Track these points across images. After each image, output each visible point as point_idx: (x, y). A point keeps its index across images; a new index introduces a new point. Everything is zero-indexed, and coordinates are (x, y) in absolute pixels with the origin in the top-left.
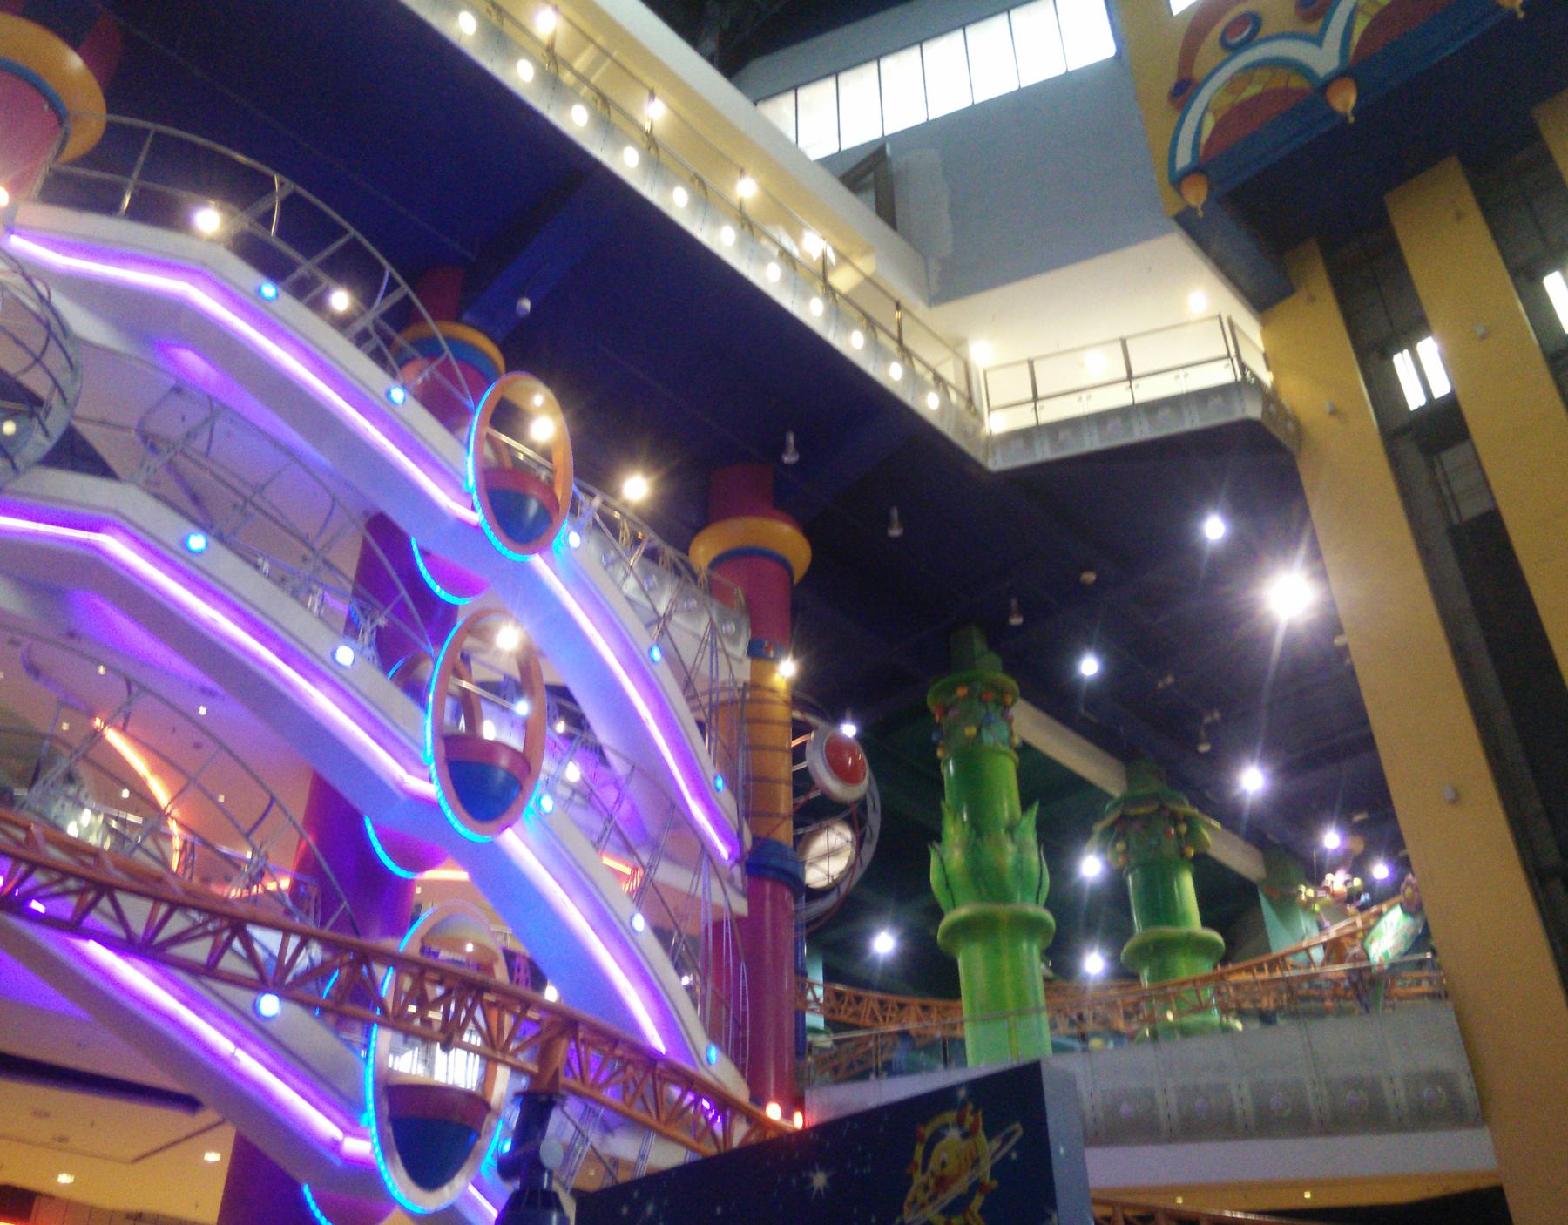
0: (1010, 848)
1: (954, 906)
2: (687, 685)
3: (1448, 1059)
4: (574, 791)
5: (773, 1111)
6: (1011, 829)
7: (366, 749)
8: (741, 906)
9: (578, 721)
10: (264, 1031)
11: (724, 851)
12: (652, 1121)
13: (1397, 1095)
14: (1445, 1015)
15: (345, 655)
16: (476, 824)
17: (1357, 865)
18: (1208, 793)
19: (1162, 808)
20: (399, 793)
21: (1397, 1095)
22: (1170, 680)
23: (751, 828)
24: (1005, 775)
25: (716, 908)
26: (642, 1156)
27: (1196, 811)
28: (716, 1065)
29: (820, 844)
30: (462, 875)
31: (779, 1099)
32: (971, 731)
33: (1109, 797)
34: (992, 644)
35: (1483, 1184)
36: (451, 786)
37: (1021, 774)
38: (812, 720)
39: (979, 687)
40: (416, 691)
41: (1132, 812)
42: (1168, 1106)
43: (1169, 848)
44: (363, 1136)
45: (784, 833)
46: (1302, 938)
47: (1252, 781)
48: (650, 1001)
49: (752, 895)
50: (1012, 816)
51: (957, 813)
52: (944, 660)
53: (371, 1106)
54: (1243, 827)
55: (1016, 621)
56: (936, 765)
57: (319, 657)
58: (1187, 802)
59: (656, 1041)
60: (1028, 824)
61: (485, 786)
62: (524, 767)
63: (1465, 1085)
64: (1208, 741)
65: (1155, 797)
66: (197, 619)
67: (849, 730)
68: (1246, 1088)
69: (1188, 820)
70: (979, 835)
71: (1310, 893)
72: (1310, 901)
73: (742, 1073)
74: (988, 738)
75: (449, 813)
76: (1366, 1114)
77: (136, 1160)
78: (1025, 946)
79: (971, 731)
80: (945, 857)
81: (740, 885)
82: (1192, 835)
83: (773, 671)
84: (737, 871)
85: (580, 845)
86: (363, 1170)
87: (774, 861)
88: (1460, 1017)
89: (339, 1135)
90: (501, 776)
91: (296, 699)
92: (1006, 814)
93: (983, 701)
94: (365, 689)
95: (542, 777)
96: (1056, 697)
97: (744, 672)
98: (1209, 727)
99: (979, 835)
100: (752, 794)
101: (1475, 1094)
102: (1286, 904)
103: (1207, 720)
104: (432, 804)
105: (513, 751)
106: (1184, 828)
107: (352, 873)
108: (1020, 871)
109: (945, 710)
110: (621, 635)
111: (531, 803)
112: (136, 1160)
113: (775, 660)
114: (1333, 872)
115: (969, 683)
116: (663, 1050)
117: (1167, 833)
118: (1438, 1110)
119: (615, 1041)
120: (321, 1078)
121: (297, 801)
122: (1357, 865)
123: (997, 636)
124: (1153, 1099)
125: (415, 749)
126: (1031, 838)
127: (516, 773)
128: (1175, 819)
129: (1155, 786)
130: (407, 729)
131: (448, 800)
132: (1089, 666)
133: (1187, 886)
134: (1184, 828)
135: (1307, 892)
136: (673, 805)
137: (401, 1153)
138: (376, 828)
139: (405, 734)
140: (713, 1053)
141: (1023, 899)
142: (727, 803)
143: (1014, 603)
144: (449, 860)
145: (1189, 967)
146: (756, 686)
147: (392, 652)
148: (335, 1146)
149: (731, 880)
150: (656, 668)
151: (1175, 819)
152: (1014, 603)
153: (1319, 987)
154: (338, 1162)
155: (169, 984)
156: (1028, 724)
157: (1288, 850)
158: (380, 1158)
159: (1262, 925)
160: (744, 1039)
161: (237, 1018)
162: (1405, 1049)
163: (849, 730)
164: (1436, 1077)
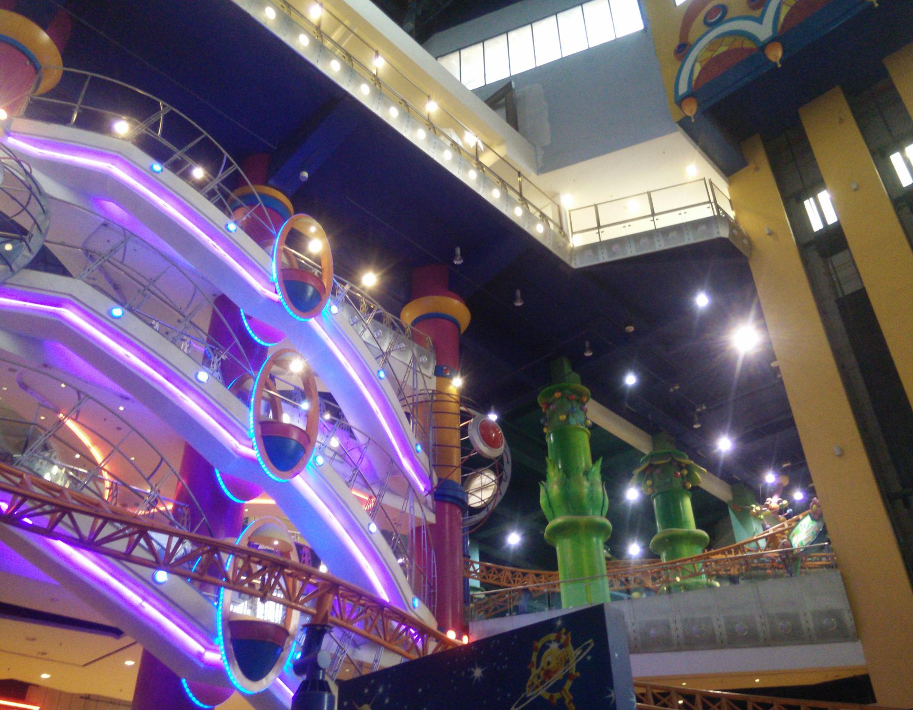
1: (554, 517)
3: (837, 602)
4: (336, 453)
5: (451, 635)
6: (586, 473)
7: (215, 430)
8: (431, 518)
9: (337, 413)
12: (382, 641)
13: (808, 623)
15: (203, 376)
17: (785, 492)
19: (673, 460)
21: (808, 623)
22: (677, 387)
23: (437, 474)
24: (583, 442)
25: (418, 519)
26: (376, 661)
28: (418, 609)
29: (477, 483)
31: (454, 628)
33: (643, 454)
34: (574, 368)
35: (858, 673)
37: (592, 441)
38: (471, 411)
39: (567, 392)
40: (244, 396)
42: (677, 631)
43: (677, 483)
46: (753, 534)
49: (438, 512)
50: (587, 465)
51: (555, 464)
53: (220, 633)
54: (720, 470)
55: (588, 354)
56: (543, 436)
58: (687, 456)
60: (596, 470)
61: (283, 449)
63: (848, 617)
64: (699, 422)
66: (118, 356)
69: (688, 467)
71: (758, 508)
72: (758, 513)
73: (433, 613)
74: (573, 421)
76: (791, 634)
78: (594, 539)
81: (430, 505)
82: (690, 477)
83: (449, 384)
84: (429, 498)
86: (216, 670)
87: (451, 493)
89: (202, 650)
92: (584, 465)
96: (611, 397)
98: (700, 414)
100: (437, 453)
101: (853, 623)
102: (744, 515)
103: (699, 410)
104: (254, 461)
106: (685, 472)
107: (208, 501)
108: (592, 498)
109: (548, 405)
111: (311, 459)
113: (450, 377)
114: (771, 497)
115: (561, 390)
117: (676, 475)
121: (176, 460)
122: (785, 492)
123: (578, 363)
124: (669, 627)
126: (598, 478)
128: (680, 467)
132: (630, 380)
133: (687, 503)
135: (756, 508)
136: (392, 461)
138: (222, 474)
140: (417, 602)
141: (594, 514)
145: (688, 551)
146: (440, 393)
147: (231, 375)
148: (200, 656)
149: (426, 504)
151: (680, 467)
152: (587, 344)
153: (763, 562)
154: (202, 665)
156: (596, 413)
157: (745, 484)
158: (226, 663)
159: (731, 527)
160: (434, 593)
162: (813, 597)
164: (831, 613)
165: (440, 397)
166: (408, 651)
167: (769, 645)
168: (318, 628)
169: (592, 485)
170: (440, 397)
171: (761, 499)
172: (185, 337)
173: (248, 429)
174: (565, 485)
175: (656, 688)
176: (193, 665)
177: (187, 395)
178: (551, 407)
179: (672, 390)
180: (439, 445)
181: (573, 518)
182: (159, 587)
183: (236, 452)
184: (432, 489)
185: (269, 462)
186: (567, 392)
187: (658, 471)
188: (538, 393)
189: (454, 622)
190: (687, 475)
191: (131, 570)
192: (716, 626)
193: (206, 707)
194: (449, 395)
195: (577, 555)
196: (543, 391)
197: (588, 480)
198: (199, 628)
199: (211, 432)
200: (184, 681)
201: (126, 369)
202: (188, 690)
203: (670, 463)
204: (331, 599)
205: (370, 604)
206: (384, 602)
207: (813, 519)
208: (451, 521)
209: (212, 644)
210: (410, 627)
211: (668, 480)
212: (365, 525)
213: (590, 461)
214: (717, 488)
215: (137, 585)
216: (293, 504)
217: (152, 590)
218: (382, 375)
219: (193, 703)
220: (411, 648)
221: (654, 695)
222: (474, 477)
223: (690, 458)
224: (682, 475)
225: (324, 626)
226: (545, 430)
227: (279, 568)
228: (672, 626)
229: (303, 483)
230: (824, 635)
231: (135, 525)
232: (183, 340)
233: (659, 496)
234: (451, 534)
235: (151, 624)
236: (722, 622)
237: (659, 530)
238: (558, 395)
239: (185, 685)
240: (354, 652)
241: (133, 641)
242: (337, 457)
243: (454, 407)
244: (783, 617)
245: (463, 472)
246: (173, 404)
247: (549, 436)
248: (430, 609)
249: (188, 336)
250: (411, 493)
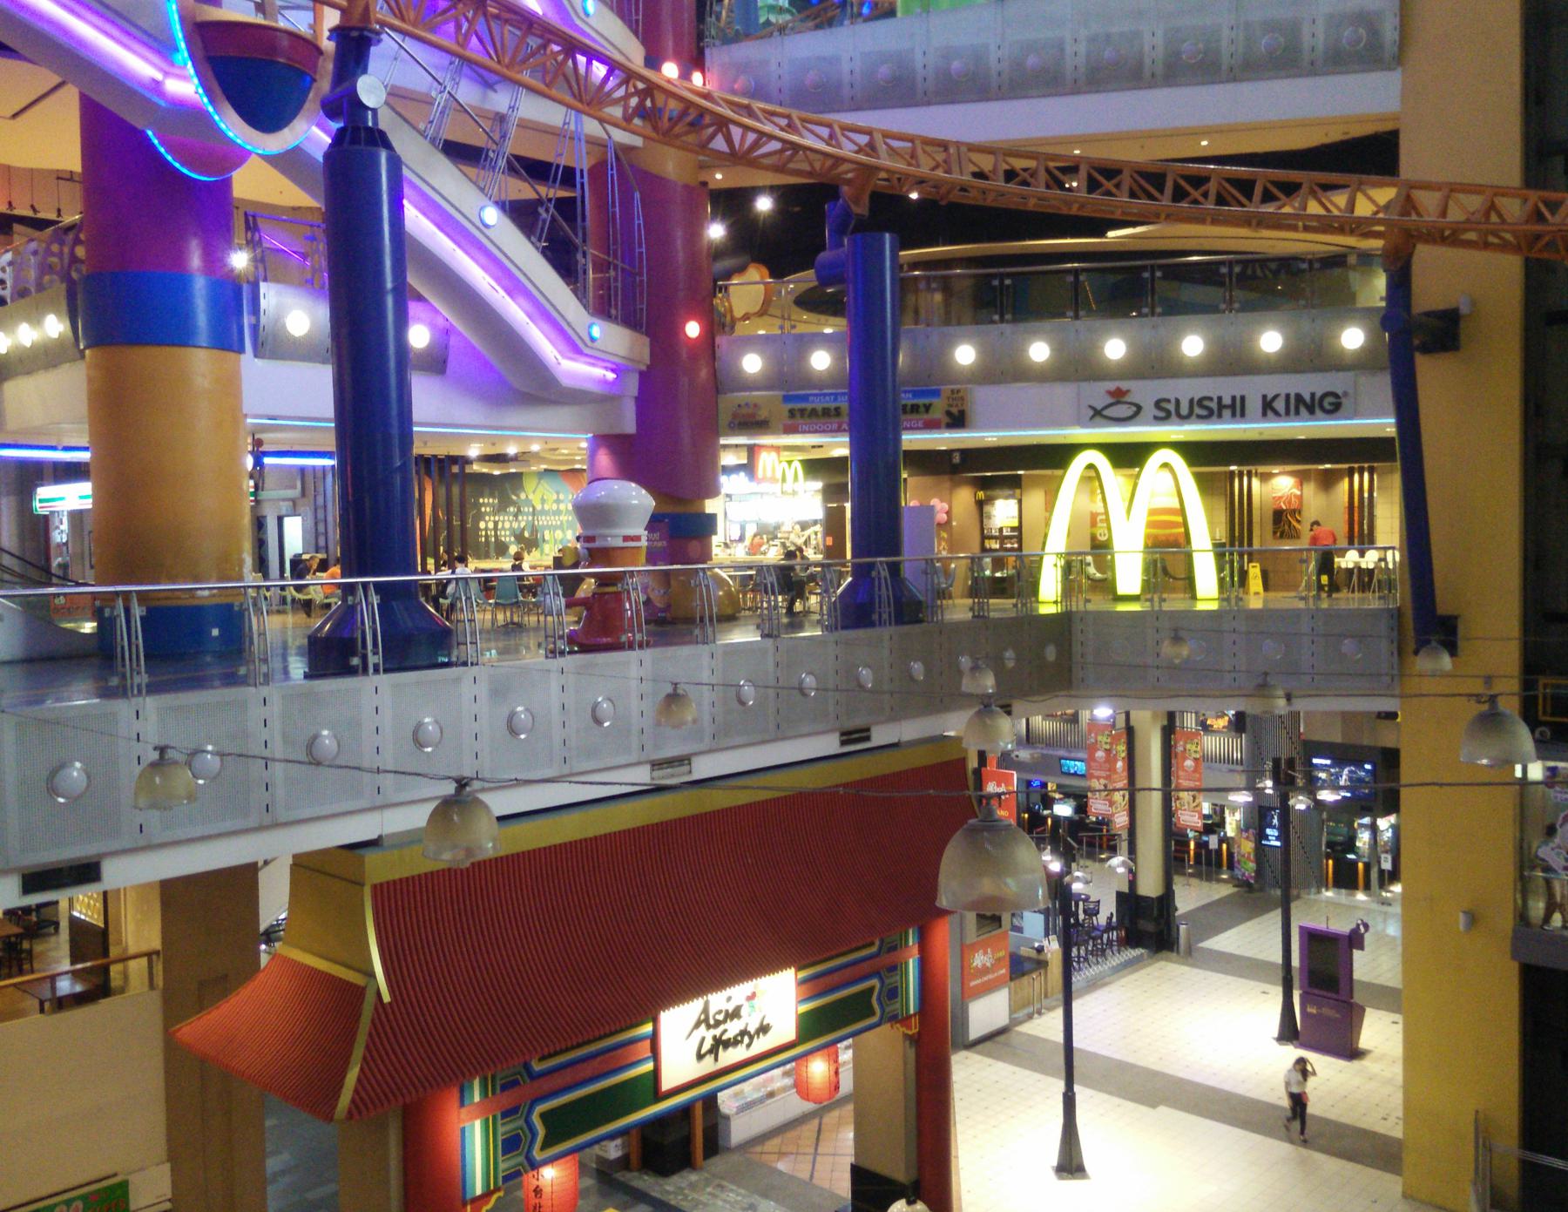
5: (670, 70)
12: (493, 64)
26: (512, 108)
31: (677, 57)
44: (185, 78)
53: (182, 45)
63: (1390, 33)
73: (636, 33)
77: (15, 116)
89: (159, 76)
112: (15, 116)
124: (1062, 50)
137: (229, 98)
148: (156, 86)
154: (162, 103)
158: (205, 100)
167: (1235, 80)
168: (355, 34)
175: (1054, 157)
189: (676, 44)
192: (1147, 48)
198: (138, 34)
206: (534, 14)
209: (172, 64)
210: (549, 41)
220: (555, 76)
221: (1048, 171)
225: (361, 29)
228: (1069, 50)
230: (1338, 60)
235: (46, 27)
236: (1159, 40)
240: (484, 97)
248: (630, 27)
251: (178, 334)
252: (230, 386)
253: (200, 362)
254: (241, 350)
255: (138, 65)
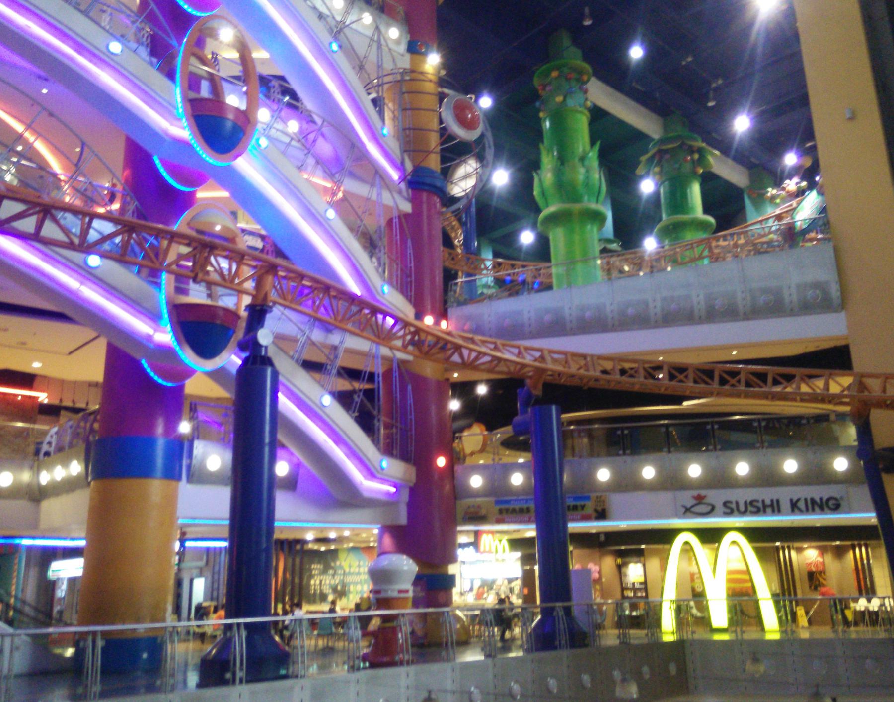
0: (582, 170)
1: (547, 206)
2: (360, 68)
3: (826, 274)
4: (292, 139)
5: (429, 320)
6: (582, 159)
7: (139, 109)
8: (407, 207)
9: (294, 96)
10: (91, 274)
11: (395, 175)
13: (791, 296)
14: (829, 249)
15: (116, 47)
16: (216, 155)
18: (714, 135)
19: (683, 144)
20: (166, 138)
21: (791, 296)
22: (690, 59)
23: (412, 160)
24: (581, 124)
25: (386, 207)
26: (341, 342)
27: (704, 145)
28: (390, 296)
29: (461, 171)
30: (225, 194)
31: (432, 313)
32: (559, 99)
33: (653, 140)
34: (575, 42)
36: (197, 132)
37: (591, 123)
38: (446, 91)
39: (566, 70)
40: (171, 75)
41: (664, 147)
42: (656, 308)
43: (687, 167)
44: (164, 332)
45: (434, 162)
46: (763, 220)
47: (742, 124)
48: (344, 263)
49: (415, 200)
50: (584, 150)
51: (550, 150)
52: (541, 52)
54: (733, 152)
55: (587, 23)
56: (539, 122)
57: (98, 49)
58: (700, 140)
59: (355, 288)
60: (593, 156)
61: (219, 130)
62: (245, 121)
63: (835, 291)
64: (714, 99)
65: (679, 137)
66: (18, 27)
67: (486, 102)
68: (702, 297)
69: (700, 151)
70: (563, 163)
71: (774, 192)
72: (773, 198)
74: (570, 102)
75: (198, 149)
76: (774, 307)
78: (589, 227)
79: (559, 99)
80: (542, 178)
81: (405, 194)
82: (702, 160)
83: (424, 61)
84: (403, 186)
85: (289, 169)
86: (165, 350)
87: (428, 181)
88: (836, 250)
90: (229, 125)
91: (90, 78)
92: (581, 149)
93: (568, 79)
94: (131, 69)
95: (259, 127)
96: (615, 73)
97: (405, 62)
98: (716, 89)
99: (563, 163)
100: (411, 139)
101: (839, 294)
102: (760, 200)
103: (714, 85)
104: (187, 144)
105: (237, 110)
106: (696, 156)
107: (154, 193)
108: (587, 184)
109: (544, 87)
110: (309, 34)
111: (253, 141)
113: (425, 55)
114: (790, 179)
115: (558, 68)
116: (359, 294)
117: (686, 160)
118: (817, 303)
119: (327, 288)
120: (134, 301)
121: (117, 155)
123: (578, 34)
124: (647, 306)
125: (171, 109)
126: (595, 163)
127: (240, 123)
128: (691, 150)
129: (680, 130)
130: (162, 95)
131: (197, 141)
132: (636, 52)
133: (695, 191)
134: (696, 156)
135: (772, 192)
136: (353, 146)
138: (161, 161)
139: (164, 100)
140: (386, 288)
141: (589, 201)
142: (394, 146)
143: (587, 10)
144: (211, 182)
145: (690, 236)
146: (414, 74)
147: (160, 52)
148: (149, 338)
149: (400, 192)
150: (335, 56)
151: (691, 150)
152: (587, 10)
154: (152, 346)
155: (31, 249)
156: (599, 93)
160: (411, 282)
161: (63, 261)
163: (486, 102)
164: (816, 285)
165: (415, 75)
166: (316, 311)
167: (748, 319)
169: (587, 171)
170: (415, 75)
171: (778, 183)
172: (105, 8)
173: (175, 108)
174: (558, 173)
176: (146, 347)
177: (102, 69)
178: (548, 88)
179: (684, 63)
180: (414, 129)
181: (566, 206)
182: (93, 271)
183: (167, 134)
184: (405, 178)
185: (209, 150)
186: (566, 70)
187: (667, 156)
188: (534, 73)
190: (699, 159)
191: (60, 255)
193: (170, 385)
194: (422, 73)
195: (570, 243)
196: (539, 71)
197: (583, 165)
199: (134, 111)
200: (143, 362)
201: (37, 48)
202: (149, 370)
203: (681, 146)
204: (269, 279)
205: (316, 285)
207: (819, 193)
208: (429, 210)
211: (677, 166)
212: (322, 212)
213: (588, 147)
214: (733, 174)
215: (73, 270)
216: (245, 195)
217: (87, 275)
218: (335, 47)
219: (155, 382)
222: (458, 165)
223: (703, 141)
224: (693, 160)
226: (541, 115)
227: (208, 249)
228: (651, 306)
229: (246, 165)
230: (806, 308)
231: (39, 204)
232: (104, 12)
233: (666, 183)
234: (429, 224)
237: (664, 216)
238: (555, 74)
239: (146, 366)
241: (94, 334)
242: (294, 143)
243: (430, 87)
244: (765, 291)
245: (444, 160)
246: (87, 81)
247: (545, 121)
249: (109, 7)
250: (378, 180)
251: (145, 471)
252: (171, 502)
253: (156, 486)
254: (179, 479)
255: (140, 326)
